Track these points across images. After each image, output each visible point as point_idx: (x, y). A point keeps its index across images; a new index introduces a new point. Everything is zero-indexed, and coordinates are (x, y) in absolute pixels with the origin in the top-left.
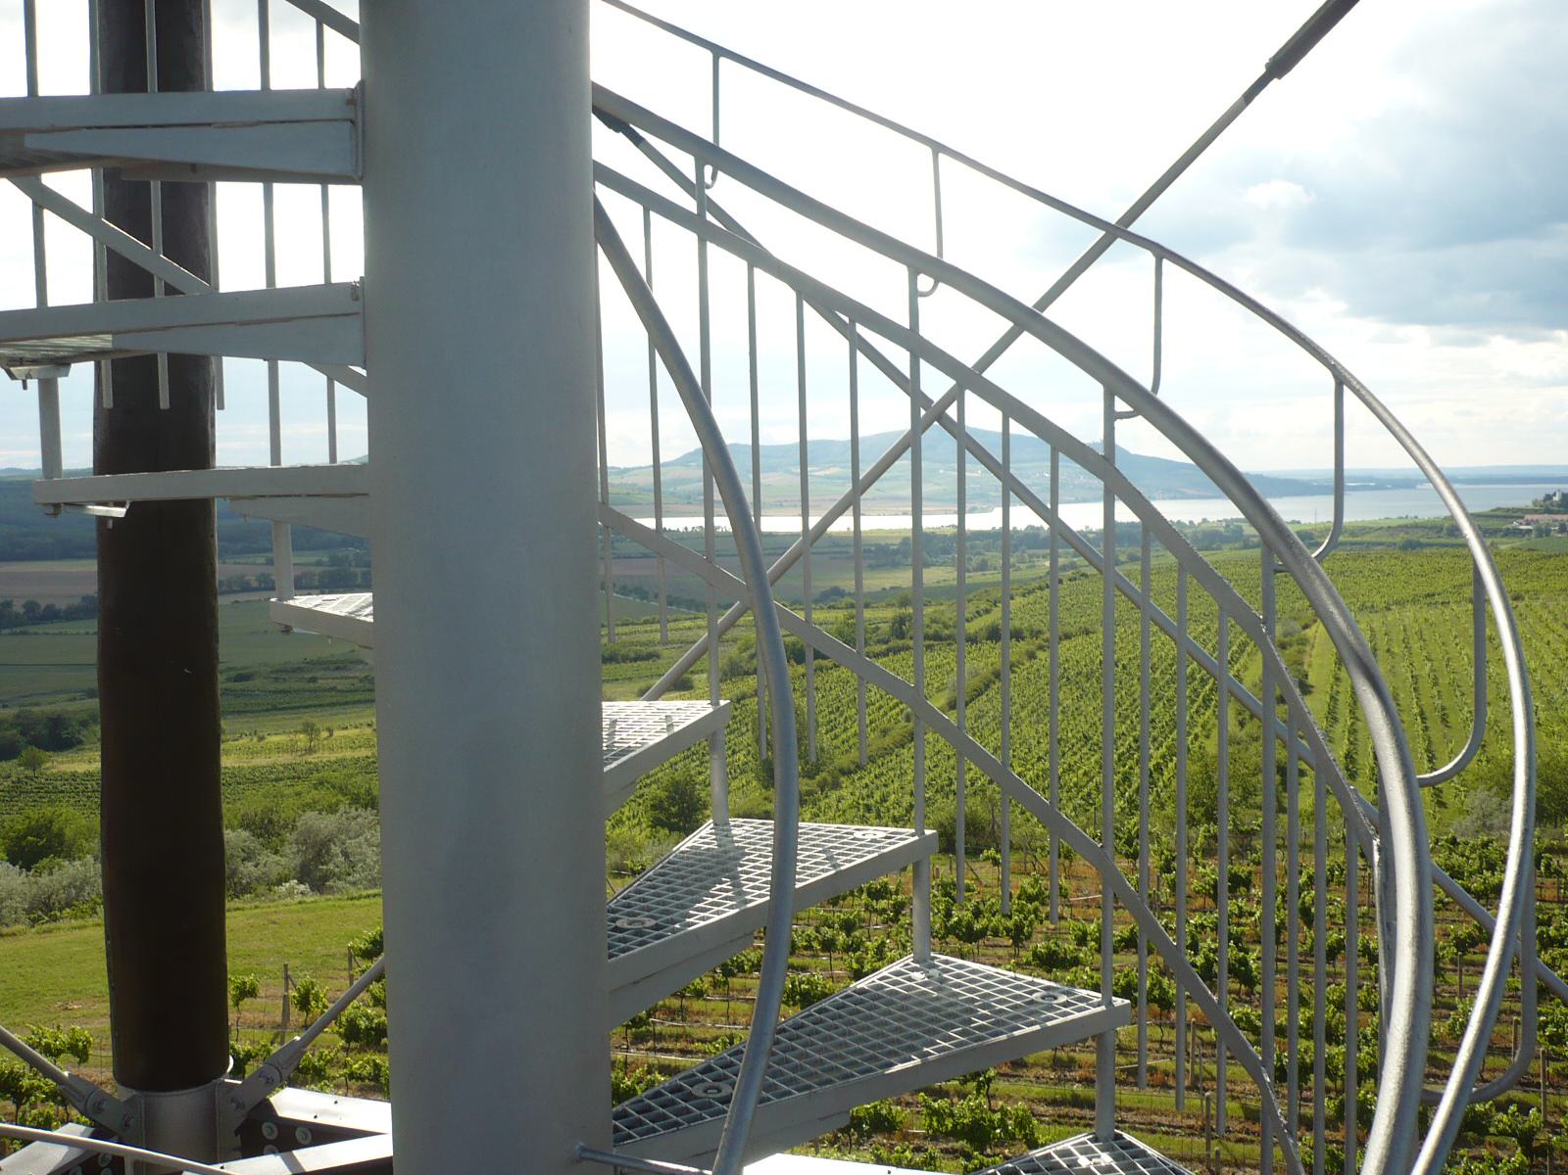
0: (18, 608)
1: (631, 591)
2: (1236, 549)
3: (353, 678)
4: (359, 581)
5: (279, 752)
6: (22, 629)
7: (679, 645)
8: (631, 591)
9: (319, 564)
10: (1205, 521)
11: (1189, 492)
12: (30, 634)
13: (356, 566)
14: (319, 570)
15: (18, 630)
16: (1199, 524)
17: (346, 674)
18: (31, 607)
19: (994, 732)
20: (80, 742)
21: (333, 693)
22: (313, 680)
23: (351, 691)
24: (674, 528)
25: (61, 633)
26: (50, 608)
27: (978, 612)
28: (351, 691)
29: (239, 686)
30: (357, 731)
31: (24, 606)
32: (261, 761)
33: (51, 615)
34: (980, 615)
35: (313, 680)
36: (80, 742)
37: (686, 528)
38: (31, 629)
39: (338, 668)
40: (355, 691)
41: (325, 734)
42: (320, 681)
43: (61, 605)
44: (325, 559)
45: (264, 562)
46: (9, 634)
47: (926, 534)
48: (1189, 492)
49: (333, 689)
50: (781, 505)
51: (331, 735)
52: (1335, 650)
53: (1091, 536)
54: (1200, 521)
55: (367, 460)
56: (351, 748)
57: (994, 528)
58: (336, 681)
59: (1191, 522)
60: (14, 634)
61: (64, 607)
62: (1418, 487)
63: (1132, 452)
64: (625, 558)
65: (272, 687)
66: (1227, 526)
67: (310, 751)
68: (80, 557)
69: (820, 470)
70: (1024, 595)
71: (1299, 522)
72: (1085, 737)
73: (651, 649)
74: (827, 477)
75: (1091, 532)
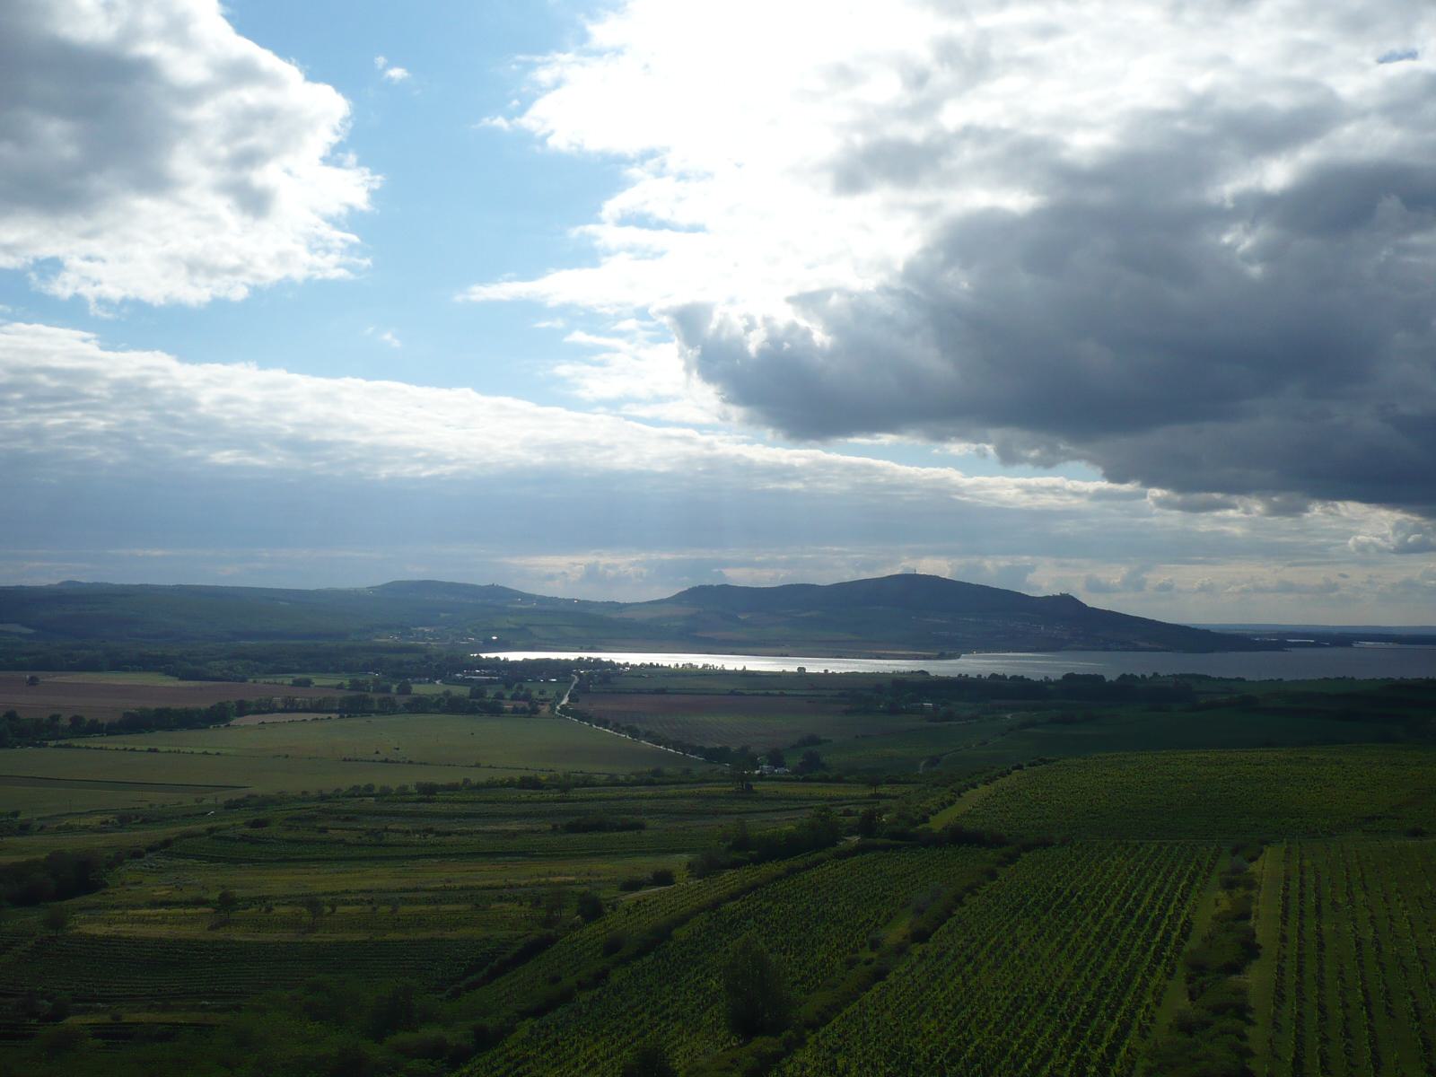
0: (65, 721)
3: (360, 830)
4: (376, 707)
5: (284, 927)
6: (67, 742)
9: (340, 687)
10: (1155, 674)
11: (1142, 644)
12: (74, 747)
13: (374, 691)
14: (339, 695)
15: (62, 742)
16: (1151, 678)
17: (354, 825)
18: (76, 721)
19: (954, 977)
20: (106, 885)
21: (342, 846)
22: (324, 830)
23: (359, 845)
24: (666, 664)
25: (101, 748)
26: (94, 722)
27: (943, 804)
28: (359, 845)
29: (256, 832)
30: (359, 907)
31: (71, 719)
32: (266, 937)
33: (94, 729)
34: (945, 807)
35: (324, 830)
36: (106, 885)
37: (677, 665)
38: (75, 742)
39: (347, 819)
40: (363, 845)
41: (328, 909)
42: (331, 831)
43: (104, 719)
44: (346, 682)
45: (291, 683)
46: (55, 747)
48: (1142, 644)
49: (341, 841)
51: (334, 911)
53: (1051, 687)
54: (1151, 675)
55: (378, 181)
56: (351, 928)
58: (345, 832)
59: (1143, 676)
60: (60, 746)
61: (106, 722)
62: (1355, 645)
65: (287, 835)
67: (312, 928)
68: (126, 670)
70: (986, 783)
71: (1243, 680)
72: (1041, 994)
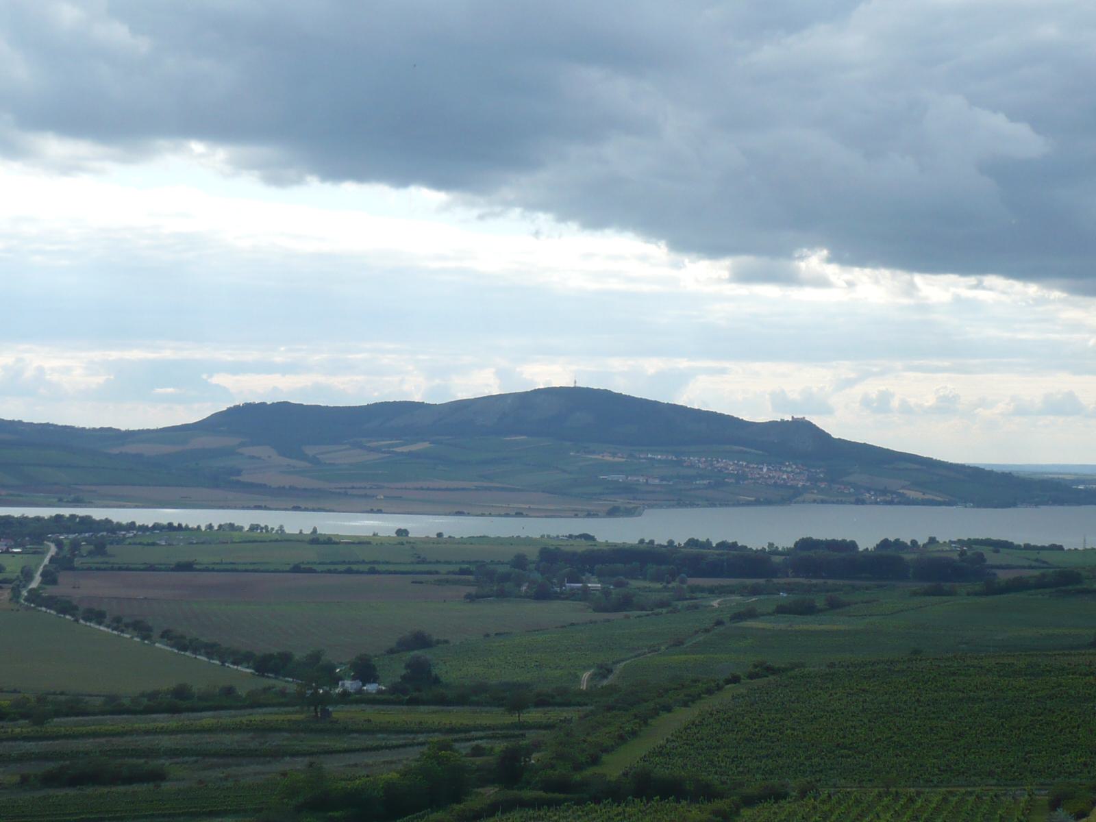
1: (127, 626)
2: (976, 594)
7: (194, 758)
8: (127, 626)
10: (932, 540)
11: (912, 494)
16: (924, 545)
47: (48, 519)
48: (912, 494)
50: (346, 494)
52: (5, 689)
54: (926, 541)
57: (671, 542)
59: (914, 542)
63: (835, 435)
64: (120, 569)
66: (963, 553)
69: (402, 445)
71: (1060, 548)
73: (155, 763)
74: (410, 454)
75: (776, 552)
